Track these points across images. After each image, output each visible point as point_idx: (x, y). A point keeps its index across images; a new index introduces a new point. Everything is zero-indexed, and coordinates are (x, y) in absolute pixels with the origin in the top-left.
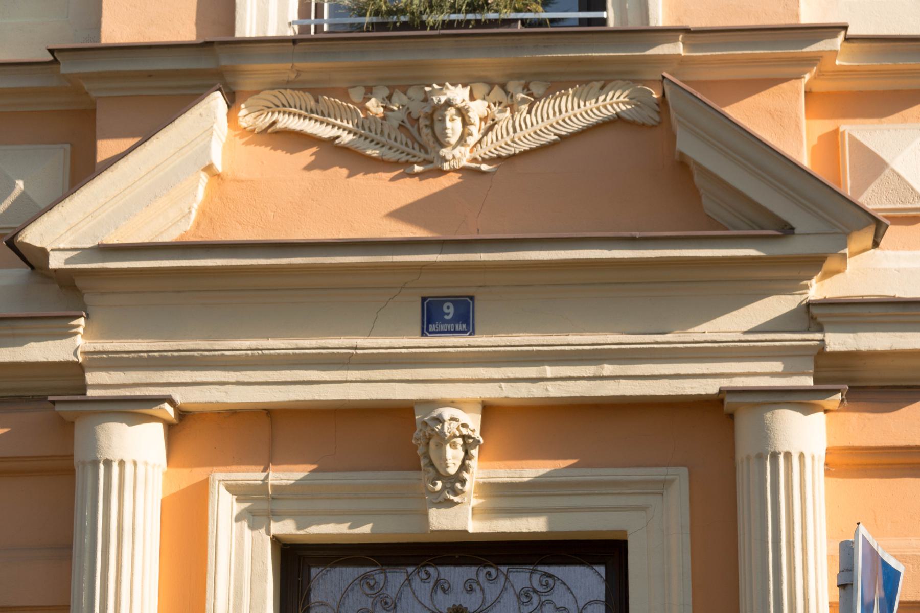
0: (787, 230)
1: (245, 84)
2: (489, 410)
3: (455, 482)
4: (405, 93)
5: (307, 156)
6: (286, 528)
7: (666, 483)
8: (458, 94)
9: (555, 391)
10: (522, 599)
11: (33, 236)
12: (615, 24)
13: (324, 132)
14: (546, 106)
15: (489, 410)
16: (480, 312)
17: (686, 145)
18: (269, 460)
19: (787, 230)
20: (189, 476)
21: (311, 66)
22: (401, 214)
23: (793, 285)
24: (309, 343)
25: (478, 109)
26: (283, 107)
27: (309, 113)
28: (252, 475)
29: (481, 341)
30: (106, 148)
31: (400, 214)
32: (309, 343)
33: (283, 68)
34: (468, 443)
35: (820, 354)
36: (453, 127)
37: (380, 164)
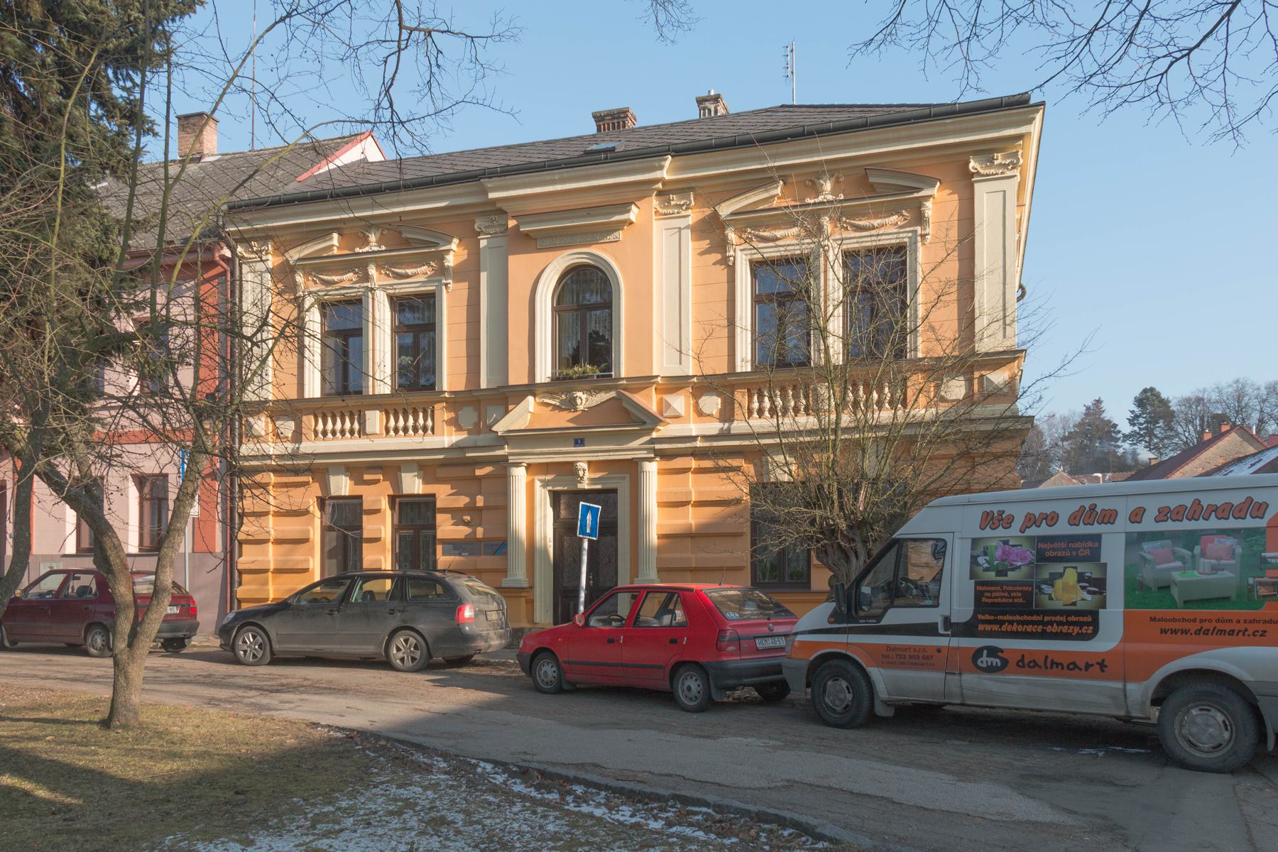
0: (644, 423)
1: (537, 392)
2: (589, 463)
3: (582, 478)
4: (273, 422)
5: (550, 408)
6: (550, 488)
7: (624, 478)
8: (579, 394)
9: (601, 458)
10: (400, 640)
11: (494, 429)
12: (489, 381)
13: (553, 402)
14: (598, 395)
15: (589, 463)
16: (586, 442)
17: (625, 404)
18: (547, 474)
19: (644, 423)
20: (531, 478)
21: (550, 389)
22: (569, 421)
23: (649, 434)
24: (551, 450)
25: (584, 397)
26: (545, 397)
27: (550, 398)
28: (543, 477)
29: (586, 448)
30: (510, 407)
31: (569, 421)
32: (551, 450)
33: (545, 389)
34: (584, 470)
35: (654, 449)
36: (579, 401)
37: (565, 409)
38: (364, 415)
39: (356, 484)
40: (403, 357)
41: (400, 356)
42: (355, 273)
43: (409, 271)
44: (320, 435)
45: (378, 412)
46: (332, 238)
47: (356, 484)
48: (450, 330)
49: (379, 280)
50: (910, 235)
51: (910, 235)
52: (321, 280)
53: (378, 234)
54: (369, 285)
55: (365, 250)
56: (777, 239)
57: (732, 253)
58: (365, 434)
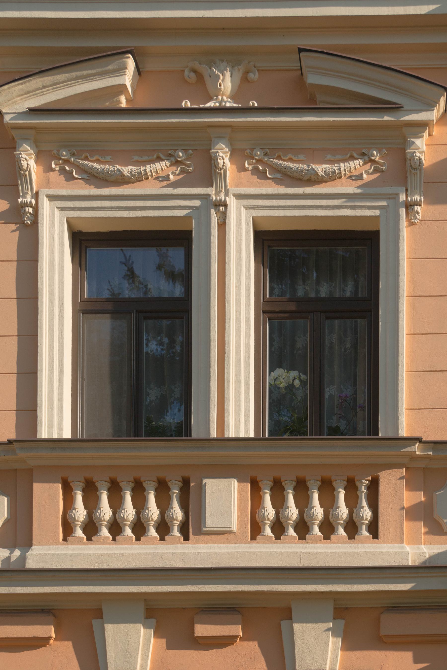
38: (201, 488)
39: (169, 647)
40: (279, 372)
41: (272, 370)
42: (177, 163)
43: (126, 170)
44: (79, 533)
45: (235, 483)
46: (123, 69)
47: (169, 647)
48: (413, 309)
49: (238, 185)
50: (197, 203)
51: (197, 203)
52: (82, 170)
53: (238, 75)
54: (211, 191)
55: (208, 105)
56: (16, 101)
57: (29, 199)
58: (199, 532)
